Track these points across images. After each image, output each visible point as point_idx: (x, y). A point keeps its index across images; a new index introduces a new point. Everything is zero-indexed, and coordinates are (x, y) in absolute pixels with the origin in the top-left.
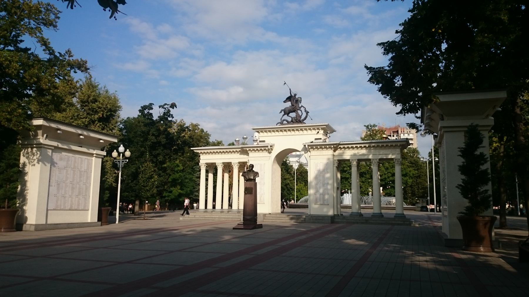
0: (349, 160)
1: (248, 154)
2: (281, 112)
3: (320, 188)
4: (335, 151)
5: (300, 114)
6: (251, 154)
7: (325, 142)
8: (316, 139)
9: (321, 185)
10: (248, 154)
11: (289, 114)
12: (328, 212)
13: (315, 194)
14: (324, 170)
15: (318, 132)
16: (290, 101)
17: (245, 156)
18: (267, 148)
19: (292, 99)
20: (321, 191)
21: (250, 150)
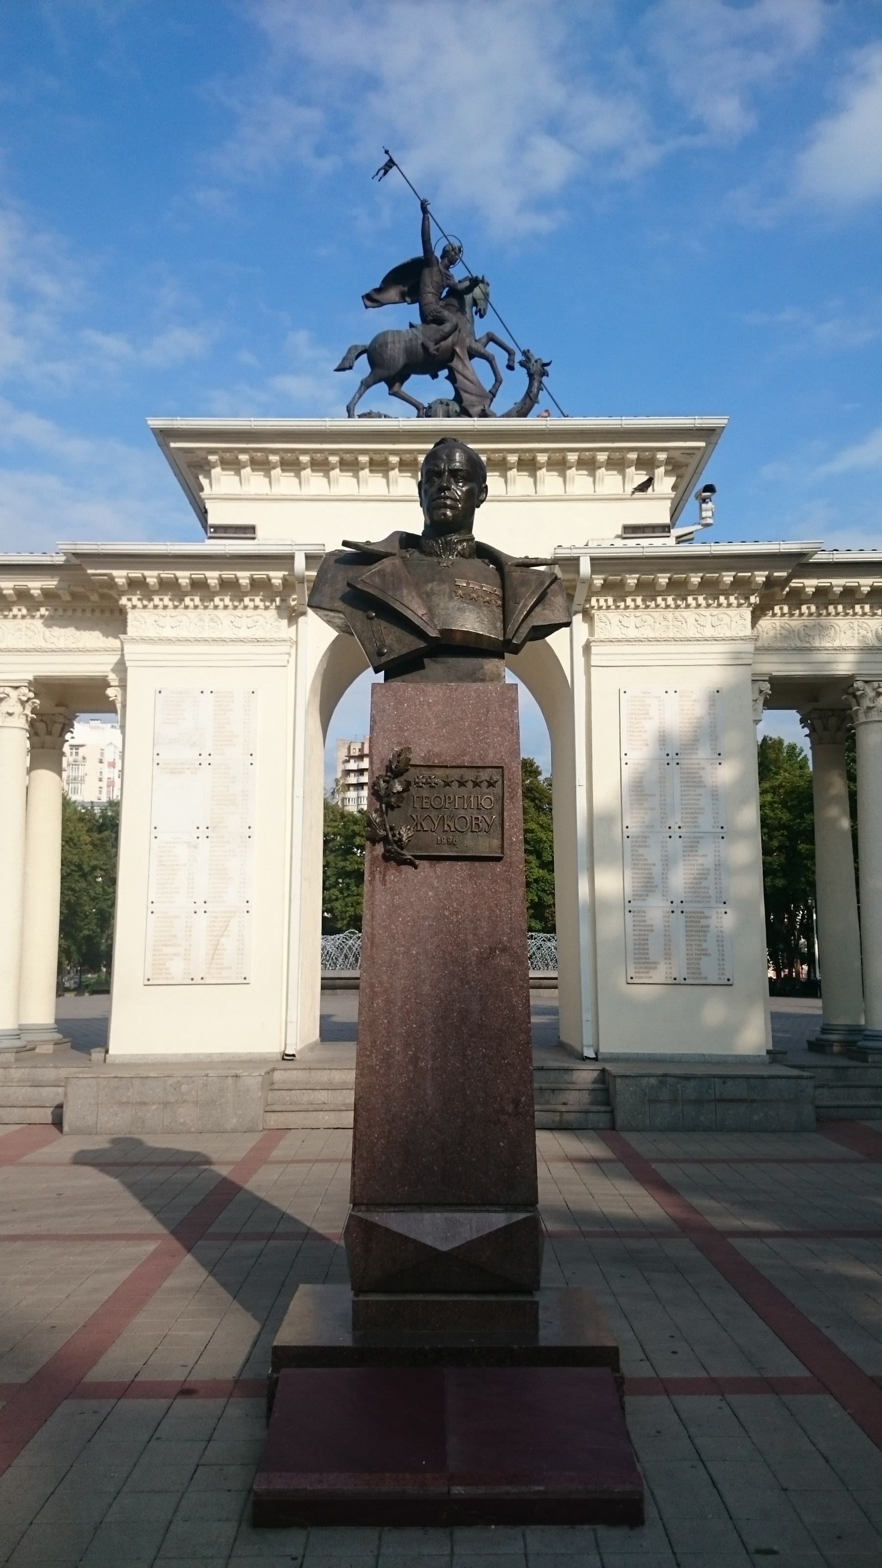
0: (845, 683)
1: (113, 619)
3: (667, 863)
4: (758, 613)
6: (142, 619)
7: (383, 654)
8: (632, 530)
9: (676, 845)
10: (113, 619)
11: (402, 376)
12: (731, 1030)
13: (631, 906)
14: (692, 743)
15: (649, 482)
16: (413, 294)
17: (93, 638)
18: (277, 576)
19: (429, 279)
20: (680, 879)
21: (135, 585)
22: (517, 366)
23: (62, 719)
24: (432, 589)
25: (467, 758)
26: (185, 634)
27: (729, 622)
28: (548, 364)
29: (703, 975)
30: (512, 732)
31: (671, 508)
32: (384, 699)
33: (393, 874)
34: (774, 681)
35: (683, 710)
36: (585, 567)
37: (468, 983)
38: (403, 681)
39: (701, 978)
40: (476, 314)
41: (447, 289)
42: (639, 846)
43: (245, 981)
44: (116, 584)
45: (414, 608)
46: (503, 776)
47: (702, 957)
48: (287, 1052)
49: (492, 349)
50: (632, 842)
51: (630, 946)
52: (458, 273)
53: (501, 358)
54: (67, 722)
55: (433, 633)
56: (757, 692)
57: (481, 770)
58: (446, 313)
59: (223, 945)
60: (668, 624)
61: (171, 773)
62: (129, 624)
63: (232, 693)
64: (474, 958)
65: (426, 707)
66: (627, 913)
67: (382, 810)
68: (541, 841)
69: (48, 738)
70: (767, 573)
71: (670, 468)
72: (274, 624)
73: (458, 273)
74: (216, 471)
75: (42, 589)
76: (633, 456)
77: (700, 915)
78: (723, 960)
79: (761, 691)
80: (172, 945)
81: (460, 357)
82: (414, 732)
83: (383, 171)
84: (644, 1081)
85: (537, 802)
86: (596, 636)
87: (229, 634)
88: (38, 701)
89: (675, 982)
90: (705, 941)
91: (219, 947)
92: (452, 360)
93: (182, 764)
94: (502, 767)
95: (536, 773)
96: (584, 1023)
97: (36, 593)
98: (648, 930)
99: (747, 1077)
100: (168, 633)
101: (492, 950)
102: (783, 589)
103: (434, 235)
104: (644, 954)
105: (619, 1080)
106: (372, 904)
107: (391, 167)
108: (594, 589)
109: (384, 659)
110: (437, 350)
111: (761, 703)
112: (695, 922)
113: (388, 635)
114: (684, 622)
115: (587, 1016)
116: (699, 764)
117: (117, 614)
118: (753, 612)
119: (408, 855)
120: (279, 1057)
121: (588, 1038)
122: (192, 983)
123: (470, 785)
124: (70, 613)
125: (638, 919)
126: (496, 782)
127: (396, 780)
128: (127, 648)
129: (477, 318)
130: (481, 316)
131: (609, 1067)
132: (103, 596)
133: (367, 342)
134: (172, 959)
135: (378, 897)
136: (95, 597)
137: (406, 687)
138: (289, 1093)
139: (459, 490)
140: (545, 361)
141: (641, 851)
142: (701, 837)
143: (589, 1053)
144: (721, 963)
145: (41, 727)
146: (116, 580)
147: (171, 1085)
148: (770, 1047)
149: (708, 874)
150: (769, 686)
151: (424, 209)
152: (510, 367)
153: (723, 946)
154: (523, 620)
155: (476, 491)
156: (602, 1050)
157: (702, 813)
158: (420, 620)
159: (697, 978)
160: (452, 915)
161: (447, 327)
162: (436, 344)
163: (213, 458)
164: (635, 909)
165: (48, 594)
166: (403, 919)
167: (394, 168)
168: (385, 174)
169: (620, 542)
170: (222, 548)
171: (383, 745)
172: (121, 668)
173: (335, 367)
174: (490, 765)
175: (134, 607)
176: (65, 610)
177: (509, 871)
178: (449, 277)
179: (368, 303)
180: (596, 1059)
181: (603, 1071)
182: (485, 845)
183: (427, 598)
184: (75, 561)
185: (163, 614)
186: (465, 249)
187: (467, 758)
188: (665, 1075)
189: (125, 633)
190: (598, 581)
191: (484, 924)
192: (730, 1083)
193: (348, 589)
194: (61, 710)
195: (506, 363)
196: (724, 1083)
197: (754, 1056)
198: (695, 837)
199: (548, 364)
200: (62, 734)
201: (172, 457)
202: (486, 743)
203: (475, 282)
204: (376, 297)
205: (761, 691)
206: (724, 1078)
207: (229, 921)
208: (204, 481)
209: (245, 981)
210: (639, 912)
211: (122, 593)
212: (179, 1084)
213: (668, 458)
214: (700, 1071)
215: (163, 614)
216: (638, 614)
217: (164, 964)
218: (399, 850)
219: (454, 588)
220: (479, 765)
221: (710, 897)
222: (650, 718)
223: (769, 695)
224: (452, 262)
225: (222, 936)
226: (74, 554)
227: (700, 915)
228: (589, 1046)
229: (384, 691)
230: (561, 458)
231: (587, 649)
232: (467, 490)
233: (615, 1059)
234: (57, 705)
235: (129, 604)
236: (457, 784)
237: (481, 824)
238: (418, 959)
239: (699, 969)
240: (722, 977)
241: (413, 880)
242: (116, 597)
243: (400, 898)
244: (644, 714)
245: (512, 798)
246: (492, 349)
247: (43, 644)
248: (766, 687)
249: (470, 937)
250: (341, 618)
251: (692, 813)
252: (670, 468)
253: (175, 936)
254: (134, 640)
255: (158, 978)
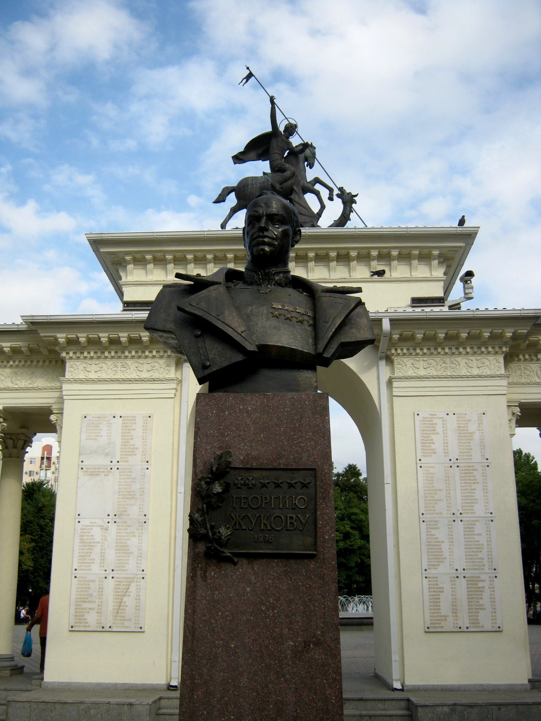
2: (221, 199)
5: (315, 207)
6: (75, 368)
8: (417, 301)
16: (261, 157)
19: (274, 143)
21: (72, 343)
22: (335, 197)
23: (24, 438)
24: (251, 311)
25: (282, 461)
26: (104, 376)
27: (489, 365)
28: (356, 196)
29: (481, 625)
30: (324, 437)
31: (444, 287)
32: (207, 407)
33: (213, 570)
34: (523, 406)
35: (460, 427)
36: (386, 325)
37: (284, 676)
38: (225, 392)
39: (479, 627)
40: (307, 166)
41: (288, 151)
42: (431, 528)
43: (141, 631)
44: (59, 342)
45: (233, 323)
46: (315, 477)
47: (480, 611)
48: (171, 684)
49: (318, 187)
50: (427, 525)
51: (427, 604)
52: (295, 141)
53: (324, 193)
54: (27, 439)
55: (251, 347)
56: (511, 414)
57: (295, 472)
58: (287, 165)
59: (125, 602)
60: (447, 365)
61: (91, 475)
62: (67, 370)
63: (135, 417)
64: (289, 652)
65: (245, 414)
66: (424, 578)
67: (203, 510)
68: (361, 521)
69: (14, 451)
70: (513, 330)
71: (442, 260)
72: (166, 368)
73: (295, 141)
74: (130, 267)
75: (11, 347)
76: (416, 252)
77: (477, 579)
78: (495, 612)
79: (514, 414)
80: (89, 602)
81: (296, 192)
82: (234, 437)
83: (245, 80)
84: (439, 709)
85: (359, 494)
86: (396, 375)
87: (134, 376)
88: (5, 424)
89: (459, 630)
90: (482, 598)
91: (122, 604)
92: (291, 194)
93: (99, 468)
94: (314, 469)
95: (358, 474)
96: (393, 663)
97: (6, 350)
98: (440, 592)
99: (516, 705)
100: (93, 376)
101: (306, 644)
102: (524, 341)
103: (279, 118)
104: (437, 609)
105: (420, 709)
106: (194, 598)
107: (250, 77)
108: (393, 341)
109: (207, 372)
110: (281, 188)
111: (514, 422)
112: (474, 584)
113: (211, 350)
114: (457, 364)
115: (395, 657)
116: (473, 466)
117: (60, 363)
118: (505, 358)
119: (227, 553)
120: (165, 687)
121: (396, 674)
122: (103, 630)
123: (285, 486)
124: (29, 363)
125: (432, 583)
126: (309, 483)
127: (217, 482)
128: (65, 387)
129: (307, 169)
130: (311, 168)
131: (415, 699)
132: (51, 351)
133: (234, 184)
134: (89, 612)
135: (199, 592)
136: (45, 352)
137: (227, 398)
138: (171, 717)
139: (276, 231)
140: (353, 194)
141: (433, 532)
142: (476, 521)
143: (397, 685)
144: (494, 614)
145: (10, 442)
146: (59, 340)
147: (83, 709)
148: (531, 677)
149: (483, 548)
150: (519, 409)
151: (272, 100)
152: (331, 199)
153: (494, 602)
154: (332, 337)
155: (291, 233)
156: (407, 683)
157: (477, 503)
158: (239, 336)
159: (476, 627)
160: (268, 609)
161: (288, 174)
162: (281, 184)
163: (128, 258)
164: (431, 576)
165: (15, 351)
166: (222, 614)
167: (253, 78)
168: (247, 82)
169: (411, 310)
170: (130, 316)
171: (206, 450)
172: (61, 400)
173: (214, 200)
174: (304, 467)
175: (71, 358)
176: (26, 361)
177: (322, 567)
178: (290, 144)
179: (236, 161)
180: (402, 690)
181: (408, 700)
182: (298, 543)
183: (247, 318)
184: (33, 328)
185: (90, 363)
186: (299, 126)
187: (282, 461)
188: (455, 704)
189: (64, 376)
190: (396, 337)
191: (298, 618)
192: (503, 709)
193: (180, 313)
194: (23, 430)
195: (328, 196)
196: (499, 709)
197: (520, 685)
198: (472, 521)
199: (356, 196)
200: (24, 448)
201: (103, 259)
202: (300, 447)
203: (306, 146)
204: (241, 157)
205: (514, 414)
206: (499, 706)
207: (130, 585)
208: (122, 274)
209: (141, 631)
210: (433, 577)
211: (63, 349)
212: (89, 708)
213: (440, 254)
214: (482, 699)
215: (90, 363)
216: (425, 359)
217: (83, 616)
218: (219, 548)
219: (272, 310)
220: (294, 467)
221: (484, 565)
222: (437, 433)
223: (519, 416)
224: (291, 134)
225: (125, 595)
226: (31, 323)
227: (477, 579)
228: (397, 680)
229: (207, 400)
230: (366, 253)
231: (390, 382)
232: (282, 231)
233: (416, 690)
234: (22, 427)
235: (67, 357)
236: (273, 486)
237: (295, 523)
238: (236, 652)
239: (477, 619)
240: (494, 625)
241: (232, 576)
242: (59, 351)
243: (219, 594)
244: (433, 430)
245: (324, 498)
246: (318, 187)
247: (10, 385)
248: (517, 410)
249: (285, 631)
250: (173, 339)
251: (470, 503)
252: (442, 260)
253: (91, 595)
254: (69, 381)
255: (79, 626)
